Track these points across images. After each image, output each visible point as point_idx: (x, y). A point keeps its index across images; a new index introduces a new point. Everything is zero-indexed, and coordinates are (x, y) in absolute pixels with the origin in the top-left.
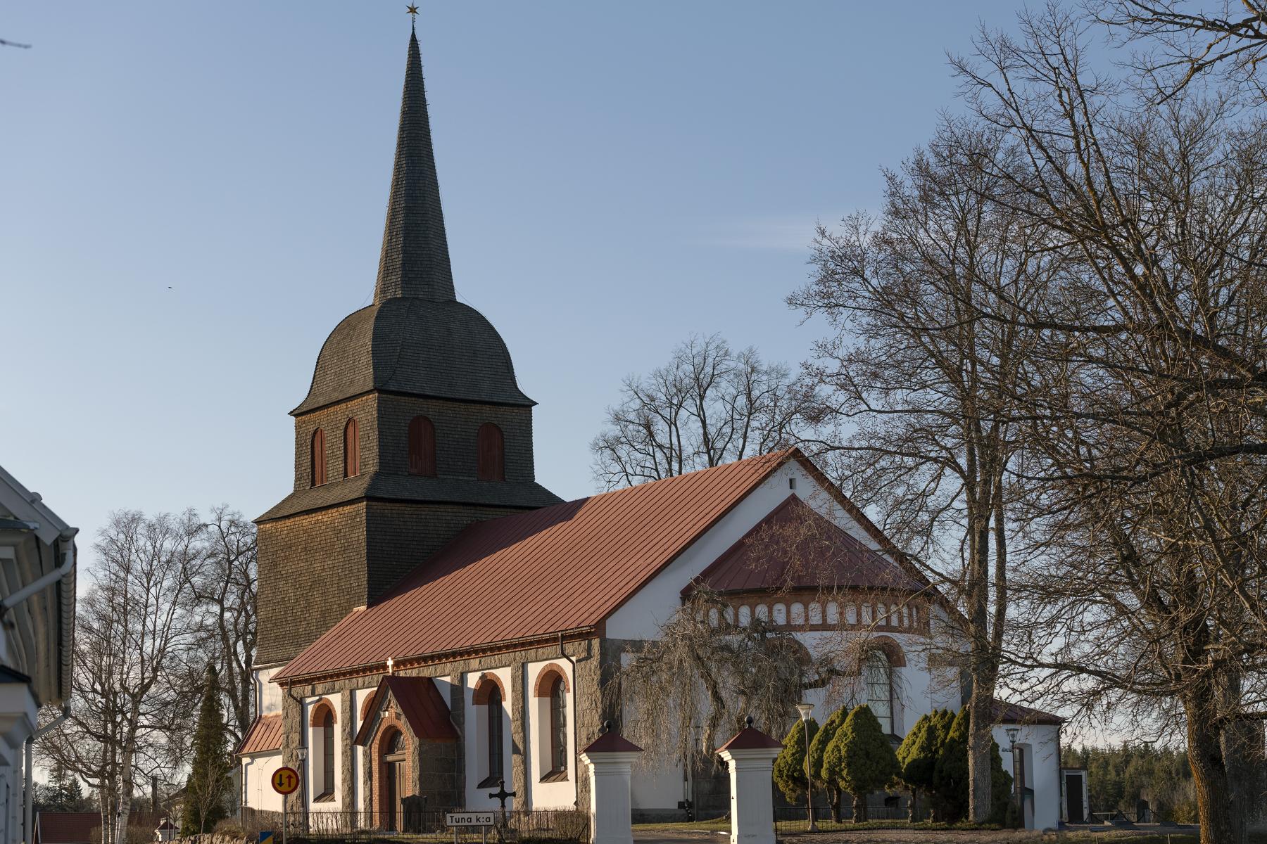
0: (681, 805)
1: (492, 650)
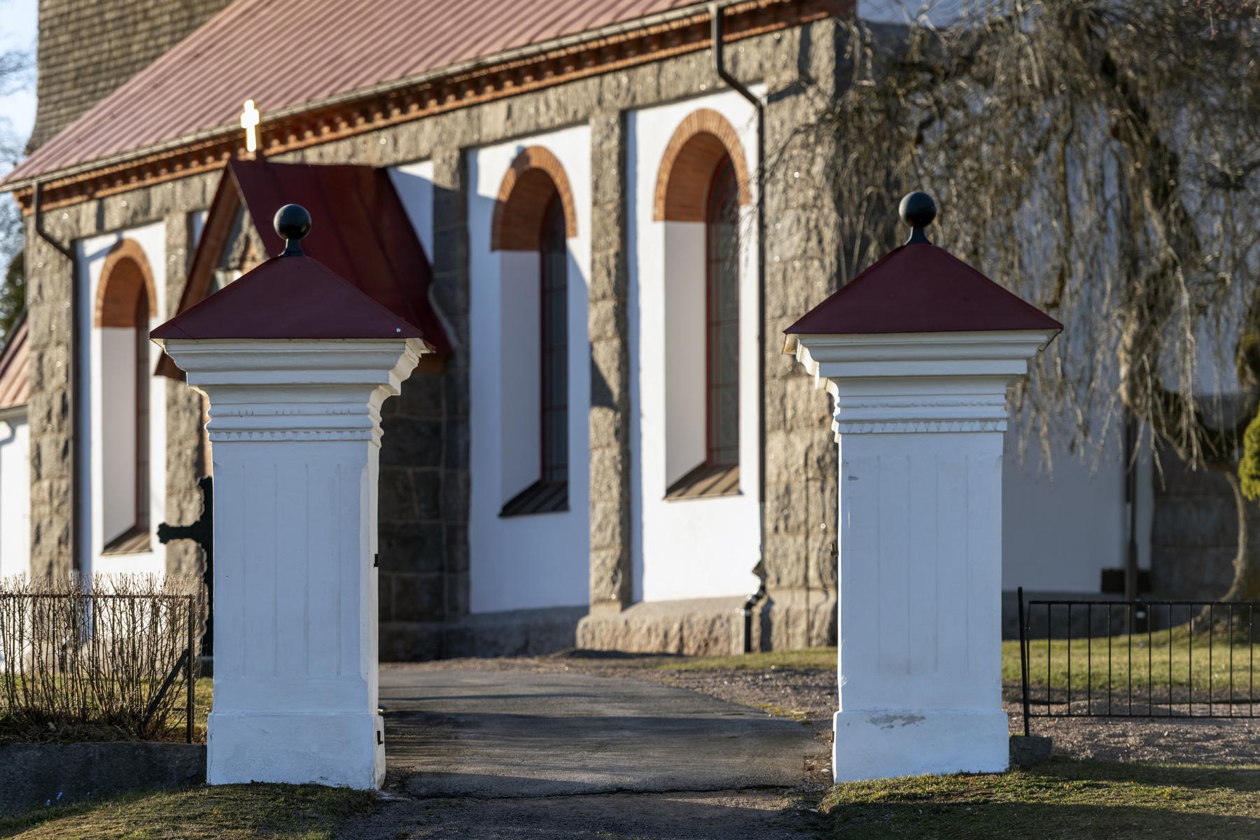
0: (1111, 580)
1: (537, 71)
